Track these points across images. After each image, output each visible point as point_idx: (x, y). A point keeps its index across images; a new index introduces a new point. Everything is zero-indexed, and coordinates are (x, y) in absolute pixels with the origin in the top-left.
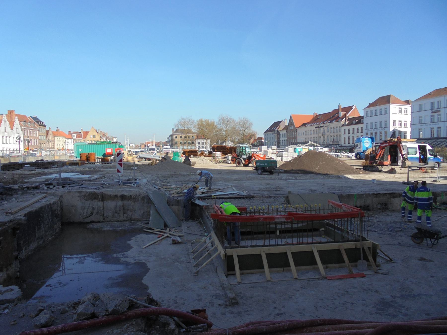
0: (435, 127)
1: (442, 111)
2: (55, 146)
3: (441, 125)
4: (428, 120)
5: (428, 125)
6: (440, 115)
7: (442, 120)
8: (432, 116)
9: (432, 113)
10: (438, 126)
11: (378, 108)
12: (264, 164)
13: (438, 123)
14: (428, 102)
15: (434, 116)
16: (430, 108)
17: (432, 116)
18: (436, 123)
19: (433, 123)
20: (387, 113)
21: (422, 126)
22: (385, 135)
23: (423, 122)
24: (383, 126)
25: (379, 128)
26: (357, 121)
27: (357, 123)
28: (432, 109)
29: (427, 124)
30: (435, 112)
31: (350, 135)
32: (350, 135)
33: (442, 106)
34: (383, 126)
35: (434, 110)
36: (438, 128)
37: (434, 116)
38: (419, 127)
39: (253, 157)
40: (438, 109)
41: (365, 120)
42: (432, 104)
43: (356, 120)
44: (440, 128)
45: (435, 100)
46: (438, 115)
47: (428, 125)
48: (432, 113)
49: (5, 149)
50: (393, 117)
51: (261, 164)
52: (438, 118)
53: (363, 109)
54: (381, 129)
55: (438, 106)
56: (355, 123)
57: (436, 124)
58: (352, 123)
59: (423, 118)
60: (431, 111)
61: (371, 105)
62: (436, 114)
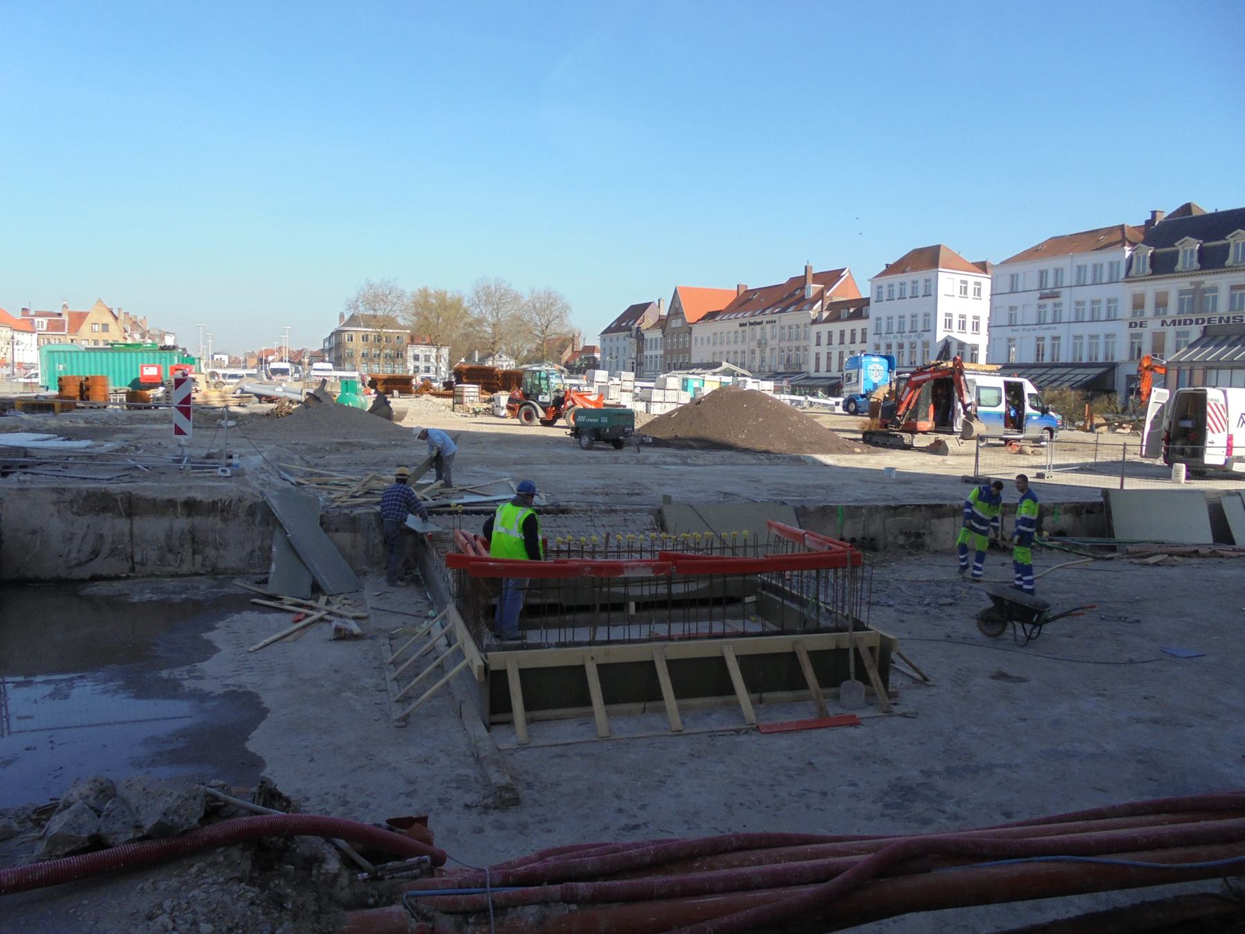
1: (1065, 293)
3: (1060, 330)
5: (1029, 330)
8: (1040, 307)
9: (1041, 298)
10: (1055, 334)
11: (908, 277)
20: (930, 292)
21: (1016, 330)
22: (924, 352)
24: (920, 327)
27: (852, 317)
34: (920, 327)
37: (1045, 306)
38: (1008, 332)
39: (568, 400)
40: (1057, 290)
41: (874, 310)
42: (1043, 274)
43: (849, 309)
45: (1050, 264)
46: (1055, 305)
48: (1041, 298)
53: (869, 280)
54: (913, 334)
57: (1049, 328)
58: (840, 316)
59: (1019, 312)
60: (1038, 294)
61: (891, 269)
62: (1050, 302)
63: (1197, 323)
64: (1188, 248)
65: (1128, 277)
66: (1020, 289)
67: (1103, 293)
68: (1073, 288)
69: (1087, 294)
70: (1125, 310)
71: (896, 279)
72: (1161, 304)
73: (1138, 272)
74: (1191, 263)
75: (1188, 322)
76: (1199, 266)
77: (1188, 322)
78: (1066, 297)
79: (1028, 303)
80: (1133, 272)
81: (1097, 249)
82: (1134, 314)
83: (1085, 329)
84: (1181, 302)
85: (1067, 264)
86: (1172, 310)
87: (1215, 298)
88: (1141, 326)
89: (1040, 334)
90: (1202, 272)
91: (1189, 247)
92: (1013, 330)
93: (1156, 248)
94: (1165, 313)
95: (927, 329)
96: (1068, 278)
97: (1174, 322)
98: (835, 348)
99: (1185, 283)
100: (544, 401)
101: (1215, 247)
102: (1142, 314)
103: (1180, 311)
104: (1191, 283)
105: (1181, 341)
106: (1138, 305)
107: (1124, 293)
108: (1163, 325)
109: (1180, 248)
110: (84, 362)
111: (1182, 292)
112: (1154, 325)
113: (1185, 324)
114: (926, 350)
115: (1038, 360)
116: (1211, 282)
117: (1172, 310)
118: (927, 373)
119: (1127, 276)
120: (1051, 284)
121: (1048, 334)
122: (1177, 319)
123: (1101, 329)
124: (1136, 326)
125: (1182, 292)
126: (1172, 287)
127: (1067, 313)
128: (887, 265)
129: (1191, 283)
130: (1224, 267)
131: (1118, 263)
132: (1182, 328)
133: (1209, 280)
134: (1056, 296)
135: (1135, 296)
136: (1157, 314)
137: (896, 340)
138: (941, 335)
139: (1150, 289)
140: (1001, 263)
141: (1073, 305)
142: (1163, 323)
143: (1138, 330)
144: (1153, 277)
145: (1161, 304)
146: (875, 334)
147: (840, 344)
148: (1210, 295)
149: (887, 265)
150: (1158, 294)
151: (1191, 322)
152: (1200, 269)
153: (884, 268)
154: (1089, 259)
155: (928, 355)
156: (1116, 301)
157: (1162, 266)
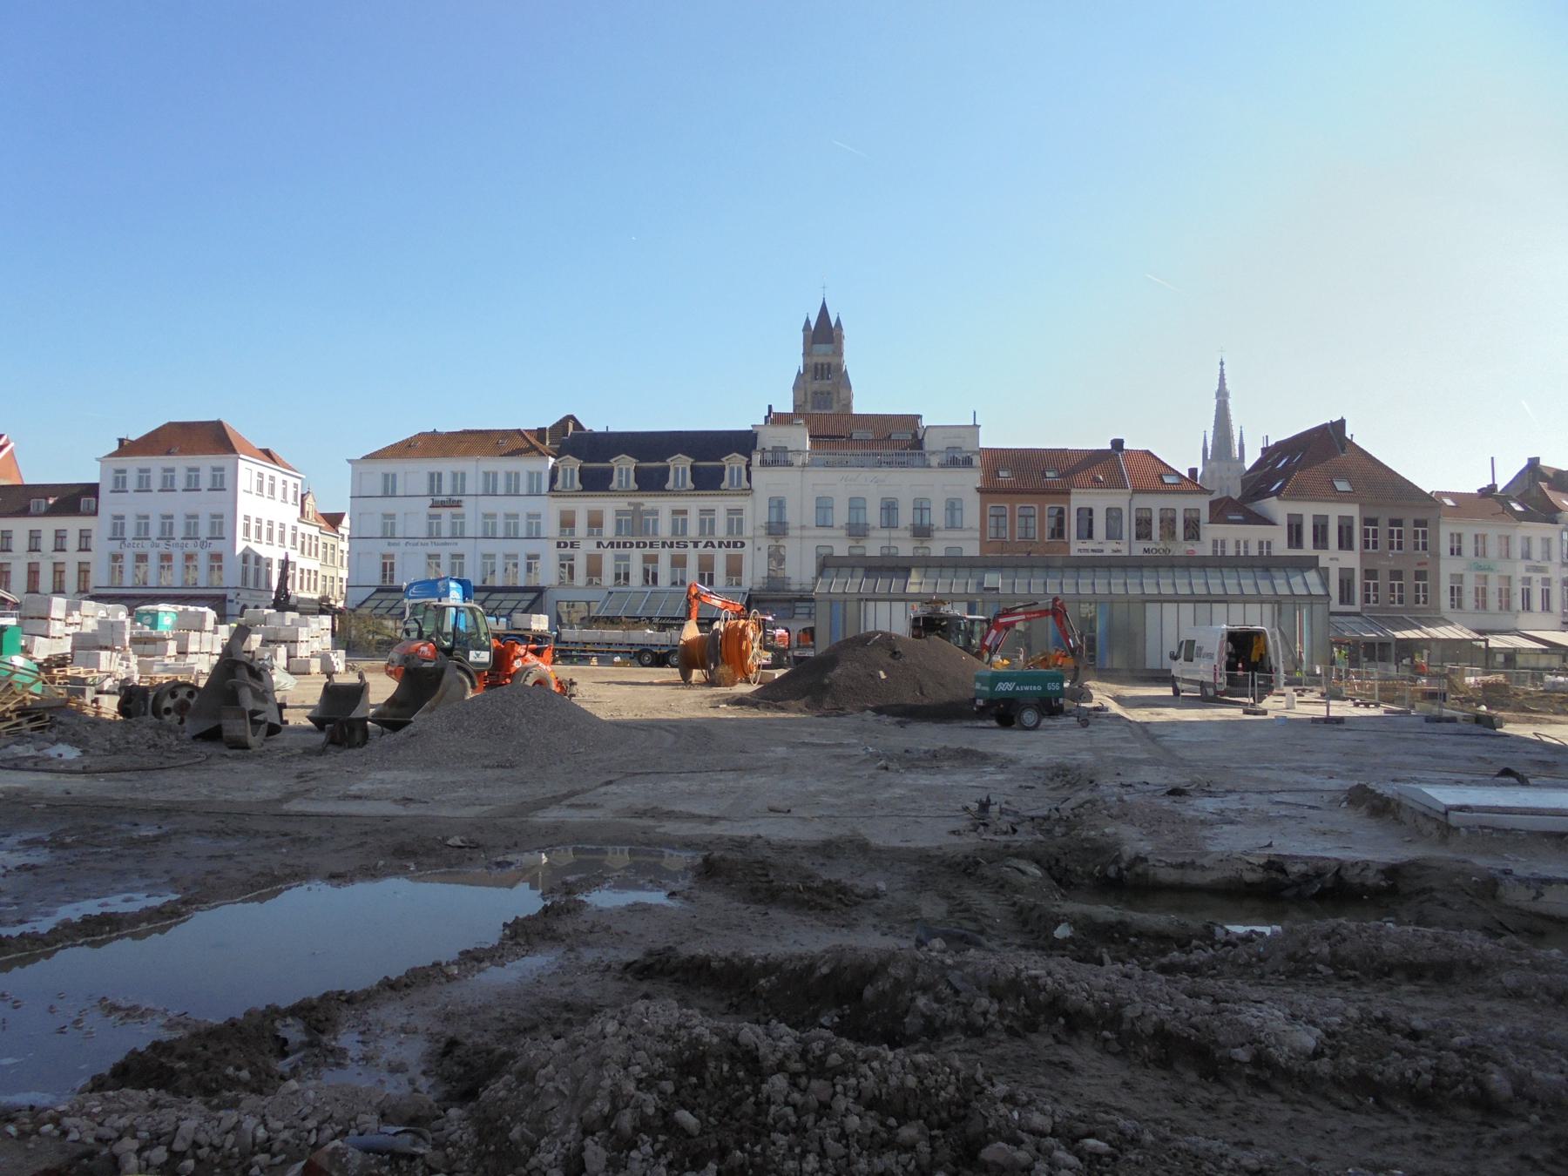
0: (445, 552)
1: (468, 503)
2: (976, 523)
3: (461, 546)
4: (419, 528)
5: (417, 544)
6: (463, 516)
7: (469, 532)
8: (431, 517)
9: (432, 506)
10: (457, 550)
11: (156, 464)
12: (1039, 688)
13: (450, 541)
14: (414, 473)
15: (438, 516)
16: (425, 490)
17: (431, 517)
18: (448, 541)
19: (436, 540)
20: (223, 484)
21: (394, 544)
22: (113, 568)
23: (399, 533)
24: (204, 532)
25: (184, 539)
26: (51, 501)
27: (53, 512)
28: (431, 494)
29: (416, 541)
30: (443, 505)
31: (13, 558)
32: (13, 558)
33: (470, 489)
34: (204, 532)
35: (440, 498)
36: (454, 556)
37: (438, 516)
38: (383, 547)
39: (516, 658)
40: (456, 498)
41: (109, 503)
42: (435, 479)
43: (47, 499)
44: (462, 556)
45: (446, 467)
46: (454, 516)
47: (417, 544)
48: (432, 506)
49: (873, 516)
50: (249, 505)
51: (1027, 688)
52: (454, 524)
53: (97, 459)
54: (191, 542)
55: (454, 487)
56: (43, 509)
57: (446, 544)
58: (28, 508)
59: (399, 521)
60: (429, 501)
61: (126, 448)
62: (446, 513)
63: (638, 547)
64: (624, 467)
65: (553, 491)
66: (399, 491)
67: (522, 506)
68: (479, 498)
69: (501, 506)
70: (551, 527)
71: (133, 464)
72: (595, 522)
73: (565, 485)
74: (684, 484)
75: (628, 545)
76: (636, 487)
77: (739, 545)
78: (469, 507)
79: (414, 514)
80: (559, 486)
81: (505, 455)
82: (562, 532)
83: (499, 548)
84: (619, 523)
85: (474, 468)
86: (609, 530)
87: (655, 521)
88: (572, 547)
89: (433, 550)
90: (696, 493)
91: (624, 466)
92: (389, 544)
93: (585, 461)
94: (600, 533)
95: (217, 535)
96: (474, 484)
97: (611, 544)
98: (19, 558)
99: (623, 503)
100: (478, 660)
101: (704, 467)
102: (572, 533)
103: (618, 532)
104: (629, 504)
105: (1394, 584)
106: (567, 522)
107: (550, 510)
108: (598, 546)
109: (726, 464)
110: (823, 537)
111: (618, 513)
112: (589, 546)
113: (625, 546)
114: (1421, 583)
115: (384, 582)
116: (653, 504)
117: (609, 530)
118: (1019, 614)
119: (551, 489)
120: (447, 489)
121: (445, 552)
122: (615, 541)
123: (522, 548)
124: (566, 546)
125: (618, 513)
126: (608, 506)
127: (473, 526)
128: (121, 441)
129: (629, 504)
130: (608, 490)
131: (539, 474)
132: (622, 551)
133: (649, 502)
134: (458, 505)
135: (730, 511)
136: (590, 534)
137: (156, 550)
138: (240, 547)
139: (582, 506)
140: (364, 458)
141: (480, 516)
142: (599, 545)
143: (568, 551)
144: (582, 493)
145: (595, 522)
146: (110, 539)
147: (31, 550)
148: (651, 518)
149: (121, 441)
150: (730, 511)
151: (632, 545)
152: (695, 489)
153: (115, 447)
154: (502, 466)
155: (121, 572)
156: (538, 516)
157: (595, 482)
